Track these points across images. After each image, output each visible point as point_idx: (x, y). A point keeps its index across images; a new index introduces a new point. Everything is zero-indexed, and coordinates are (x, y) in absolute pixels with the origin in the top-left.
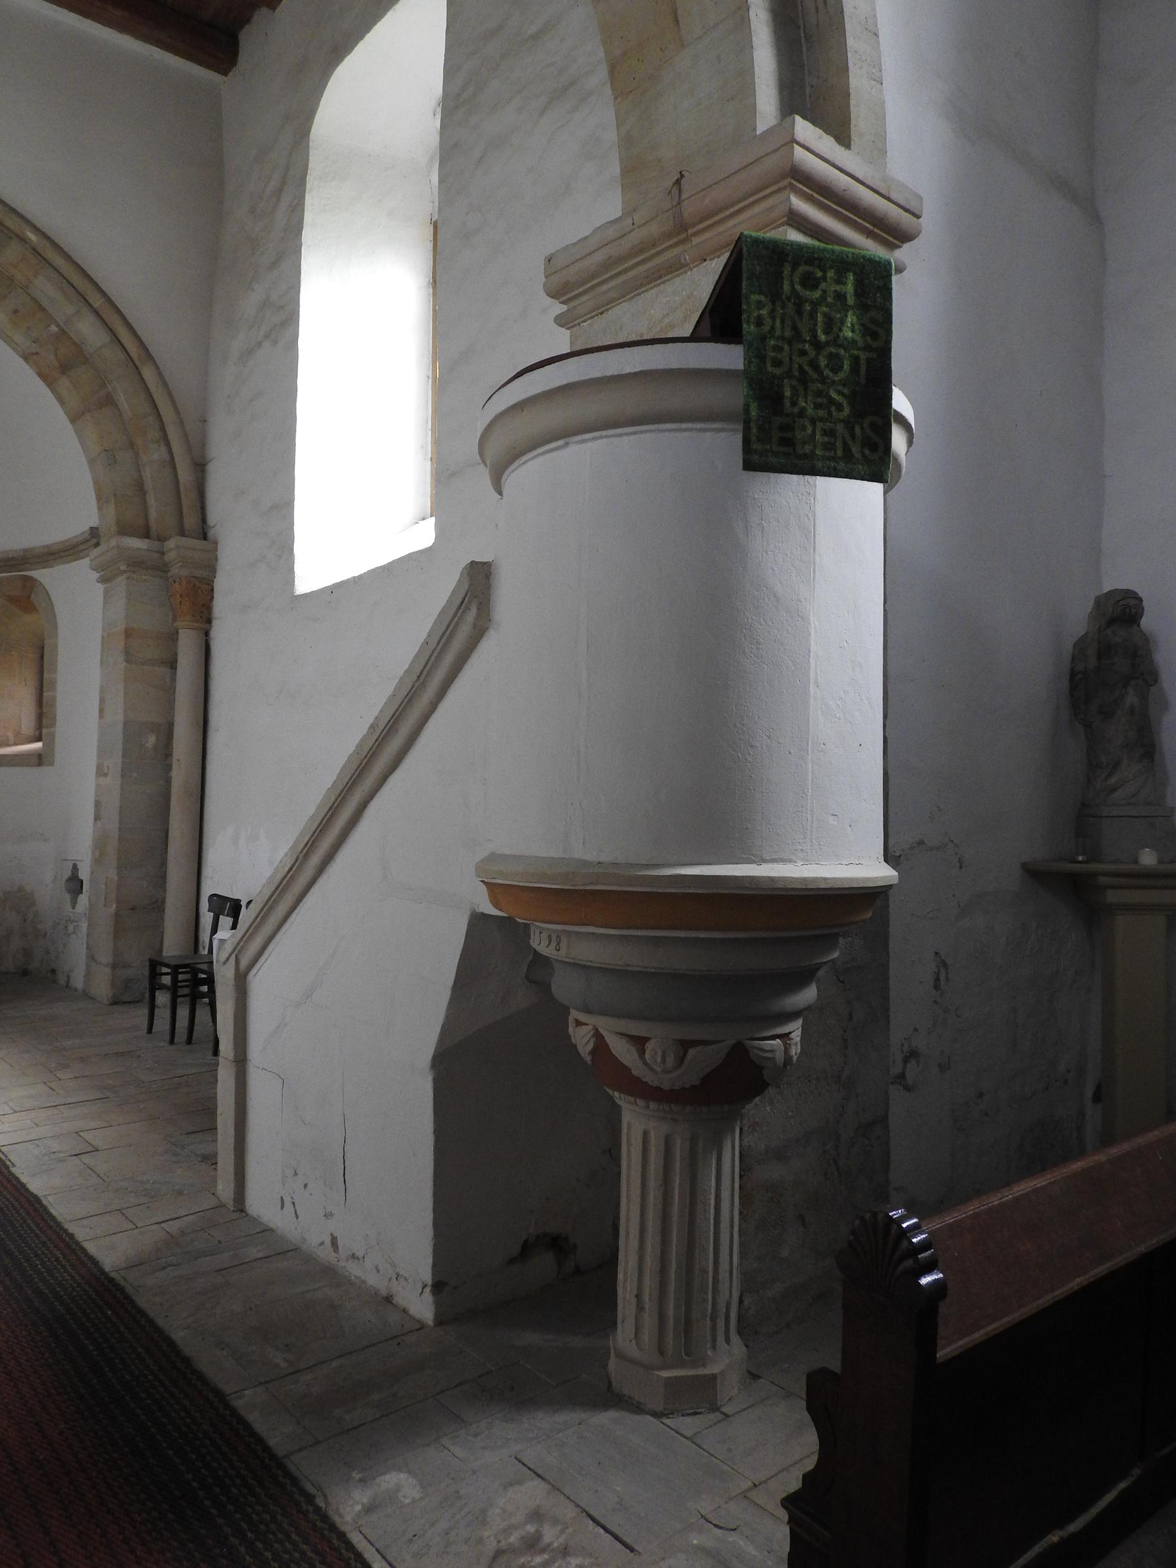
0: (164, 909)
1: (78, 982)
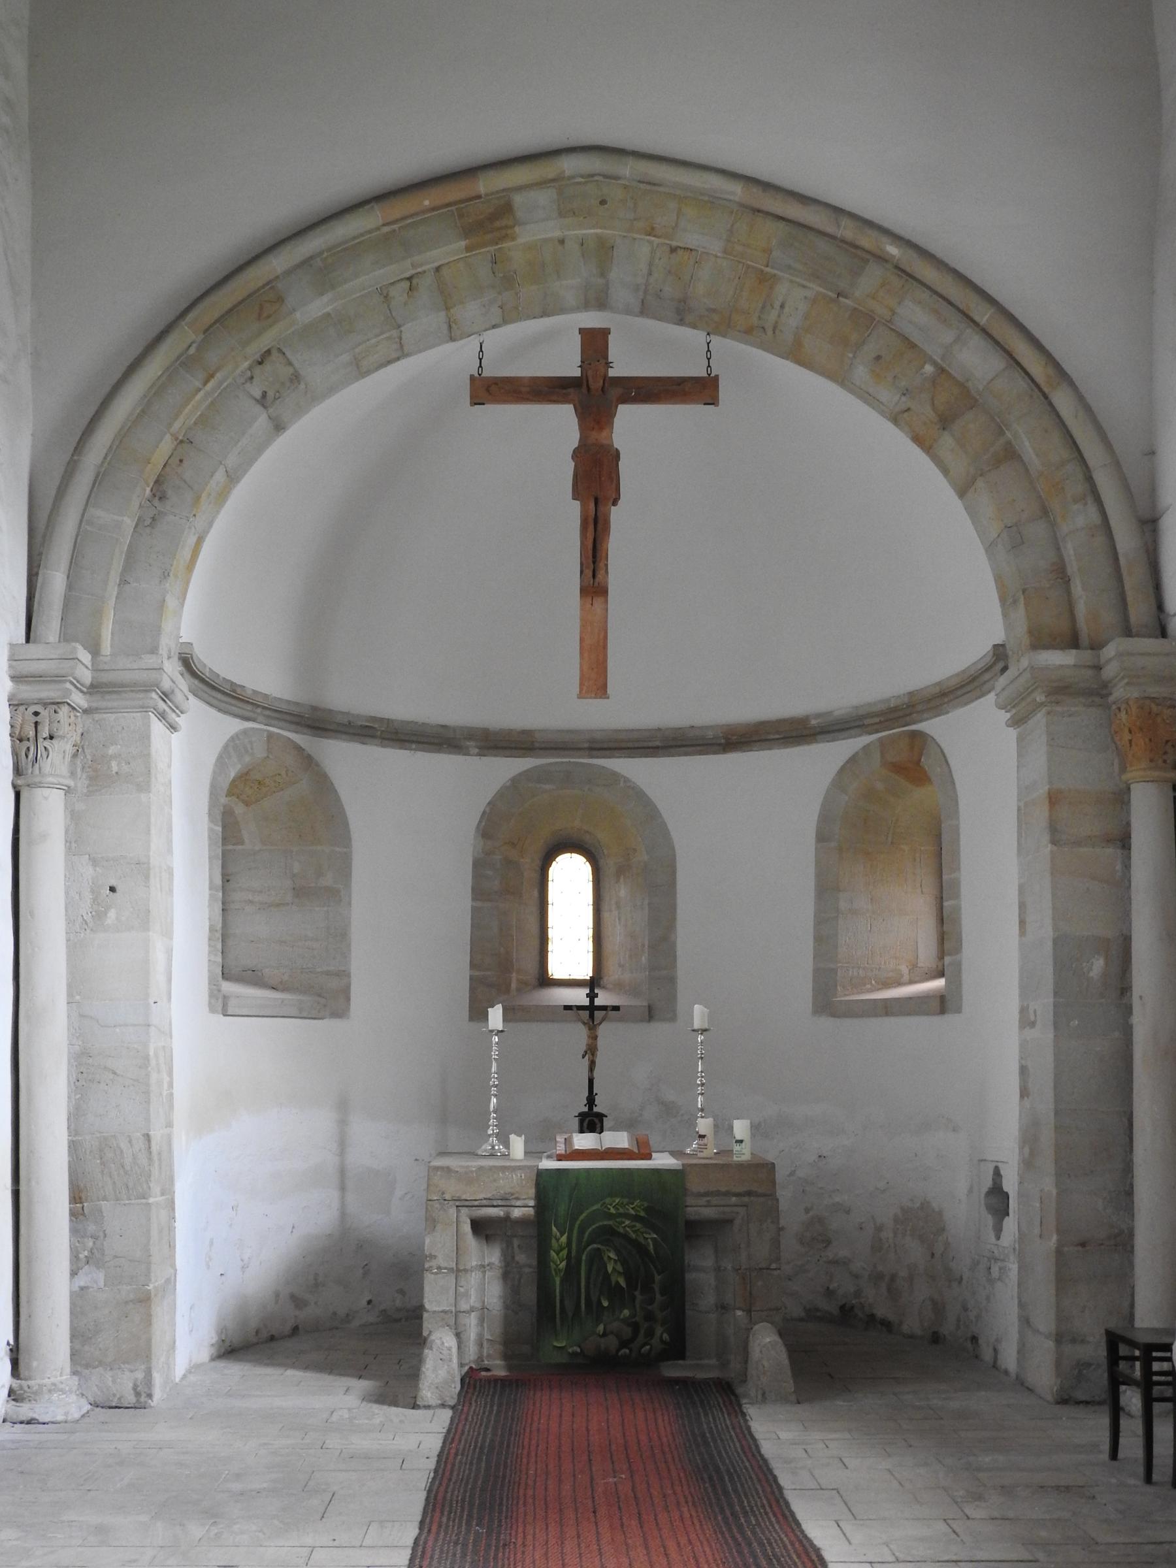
0: (1133, 1247)
1: (1009, 1359)
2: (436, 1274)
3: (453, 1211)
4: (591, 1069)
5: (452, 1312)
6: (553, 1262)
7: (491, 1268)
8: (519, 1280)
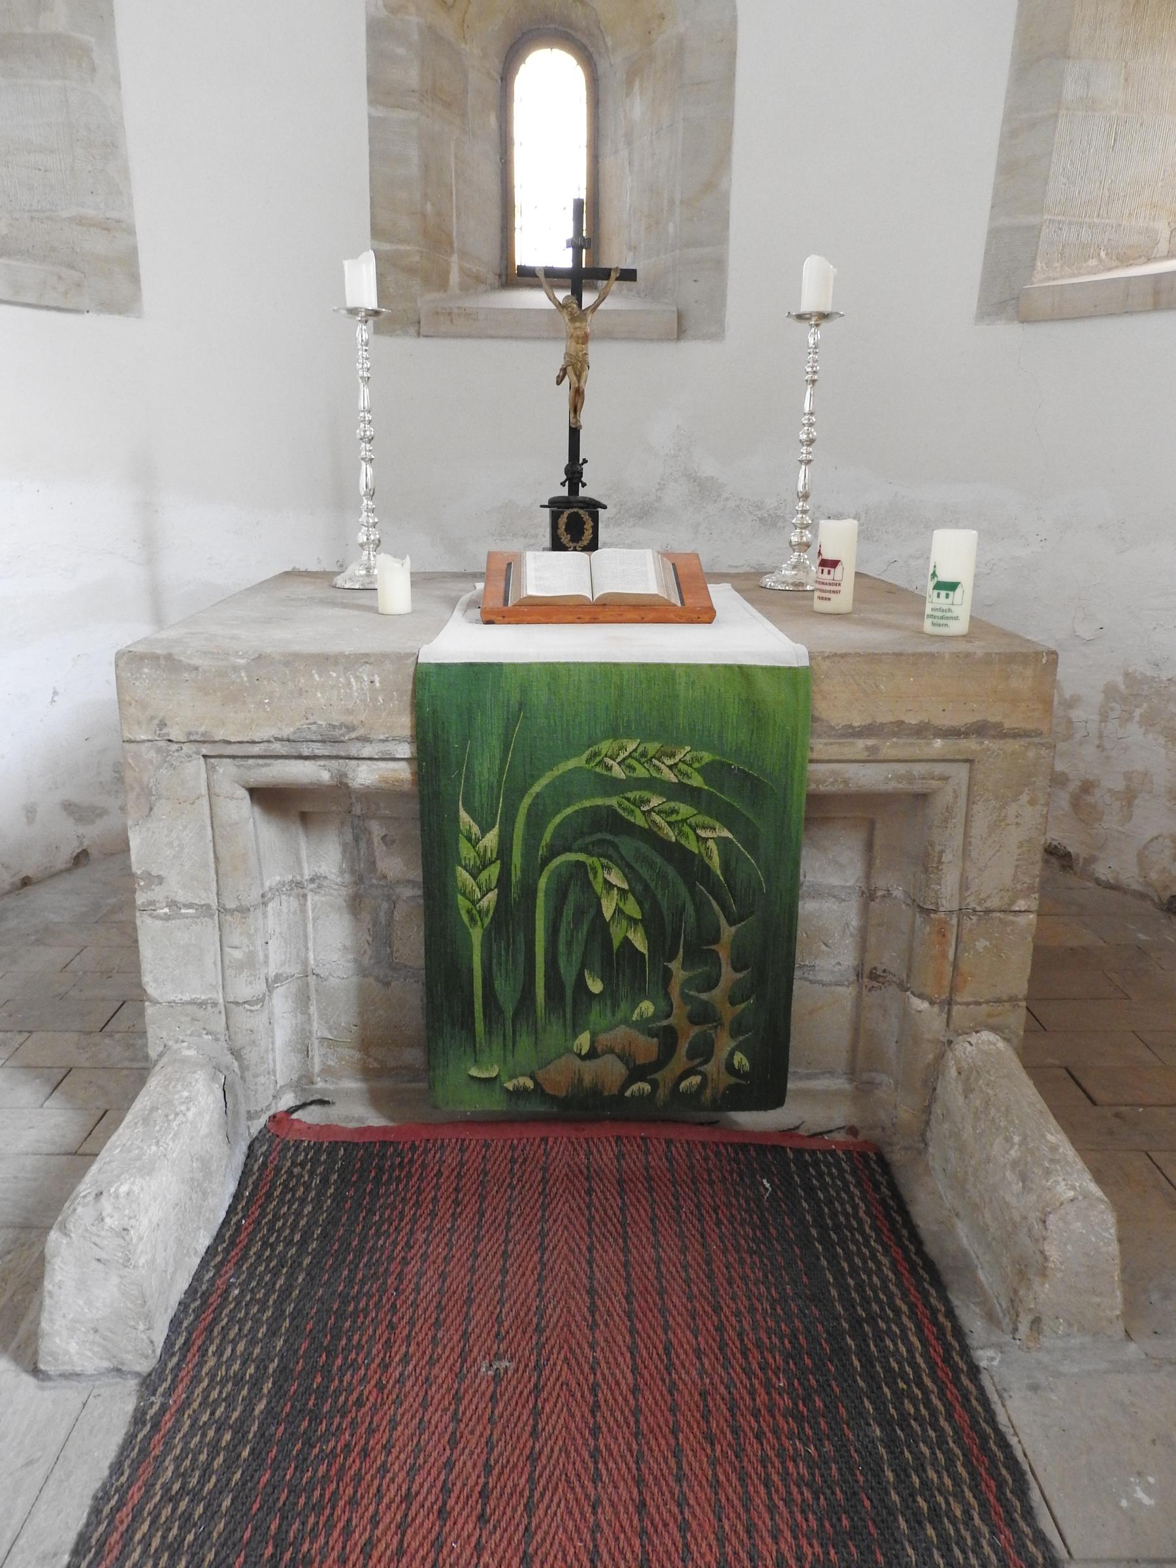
2: (167, 918)
3: (196, 769)
4: (575, 409)
5: (215, 1004)
6: (464, 894)
7: (320, 886)
8: (391, 913)
